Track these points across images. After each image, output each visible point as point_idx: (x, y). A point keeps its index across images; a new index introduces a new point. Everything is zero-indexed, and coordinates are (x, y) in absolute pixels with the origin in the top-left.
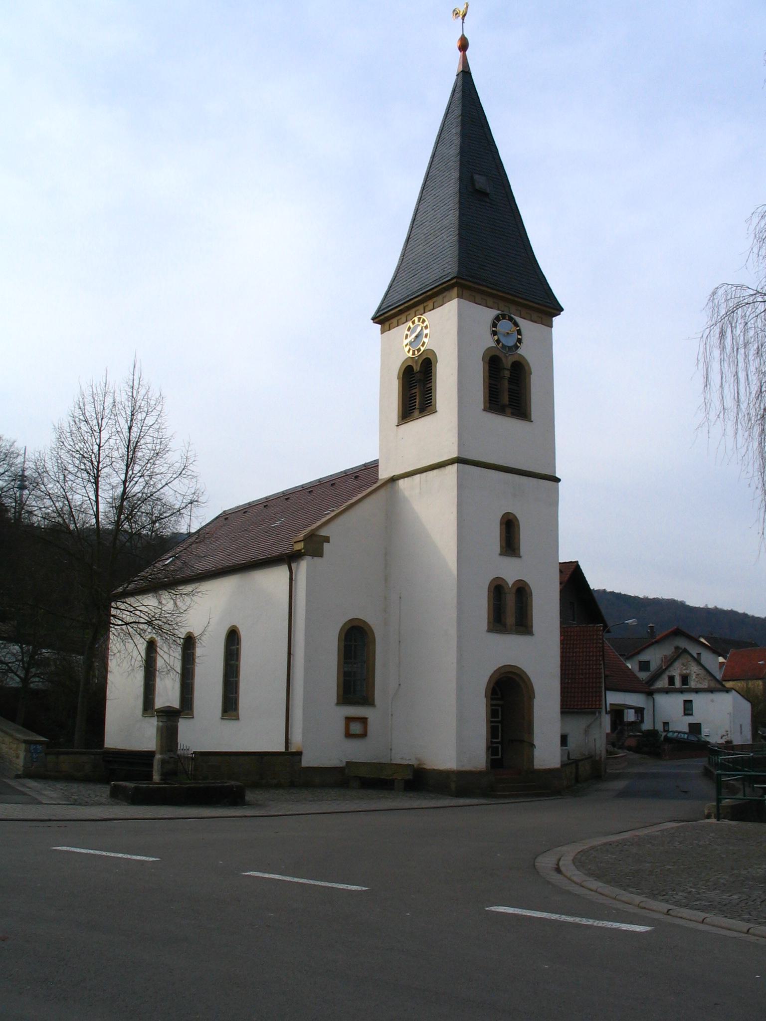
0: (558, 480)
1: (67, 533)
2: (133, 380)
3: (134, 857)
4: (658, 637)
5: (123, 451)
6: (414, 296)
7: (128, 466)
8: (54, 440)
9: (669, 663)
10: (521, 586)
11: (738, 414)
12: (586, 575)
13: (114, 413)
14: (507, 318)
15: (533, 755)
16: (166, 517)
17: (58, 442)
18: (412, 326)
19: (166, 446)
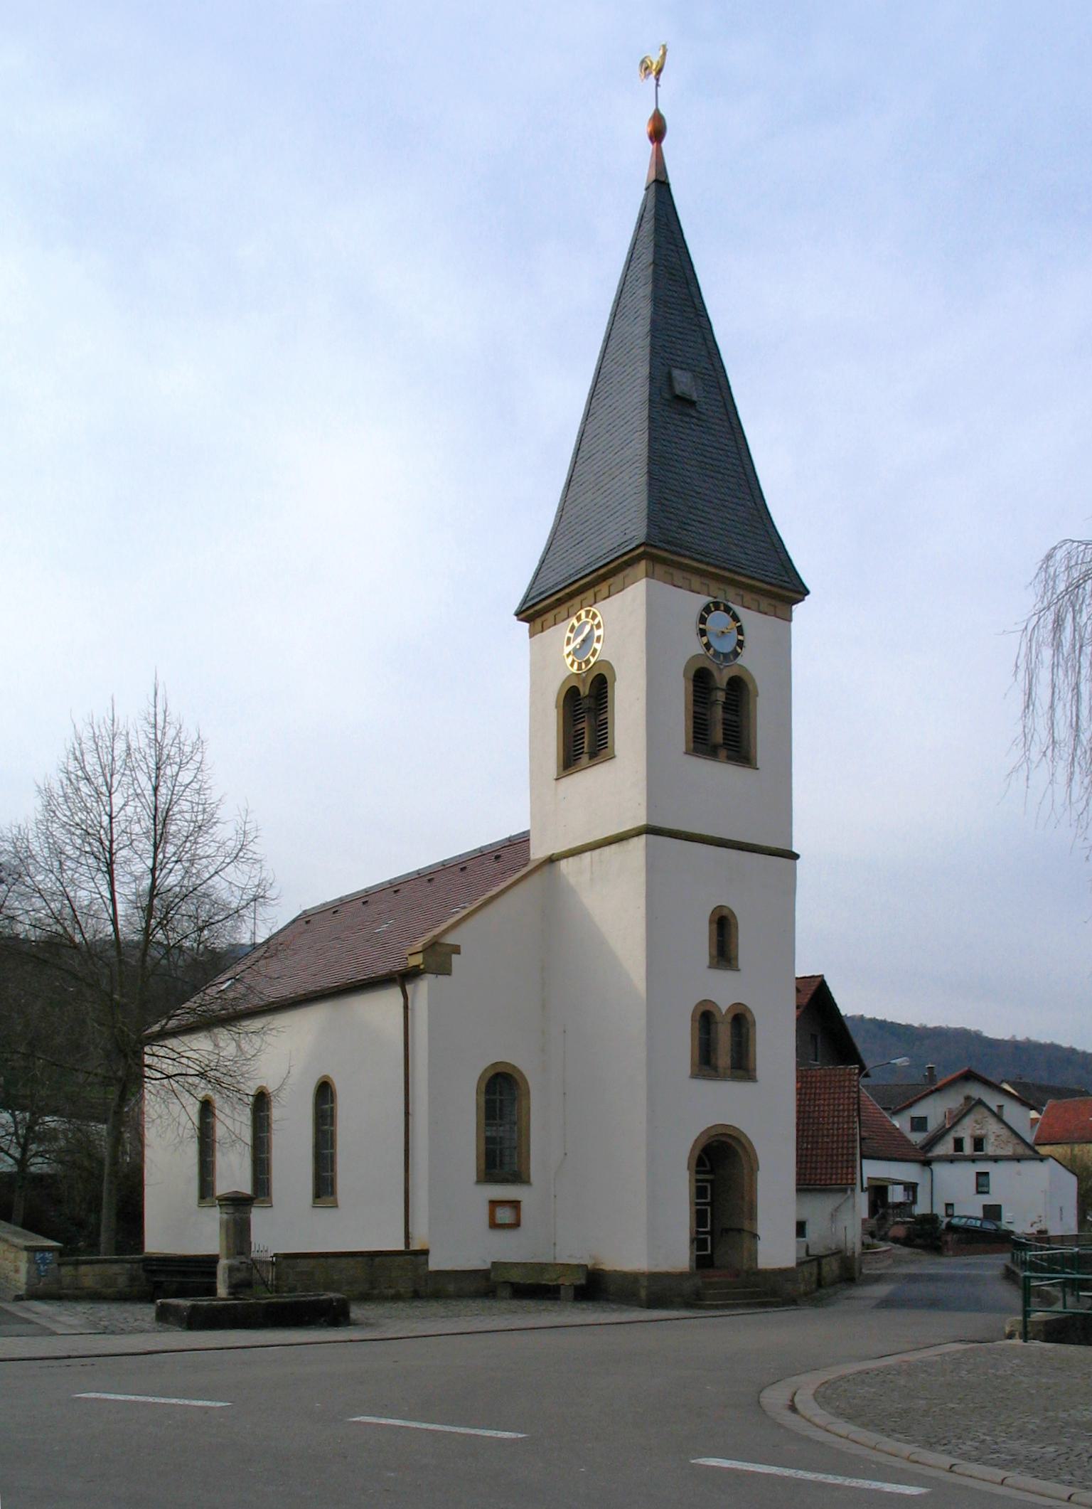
0: (795, 856)
1: (70, 947)
2: (155, 715)
3: (195, 1403)
4: (939, 1083)
5: (148, 823)
6: (579, 576)
7: (156, 847)
8: (40, 808)
9: (955, 1120)
10: (739, 1012)
11: (1075, 749)
12: (834, 995)
13: (129, 767)
14: (722, 608)
15: (756, 1250)
16: (218, 922)
17: (47, 811)
18: (576, 625)
19: (212, 815)
